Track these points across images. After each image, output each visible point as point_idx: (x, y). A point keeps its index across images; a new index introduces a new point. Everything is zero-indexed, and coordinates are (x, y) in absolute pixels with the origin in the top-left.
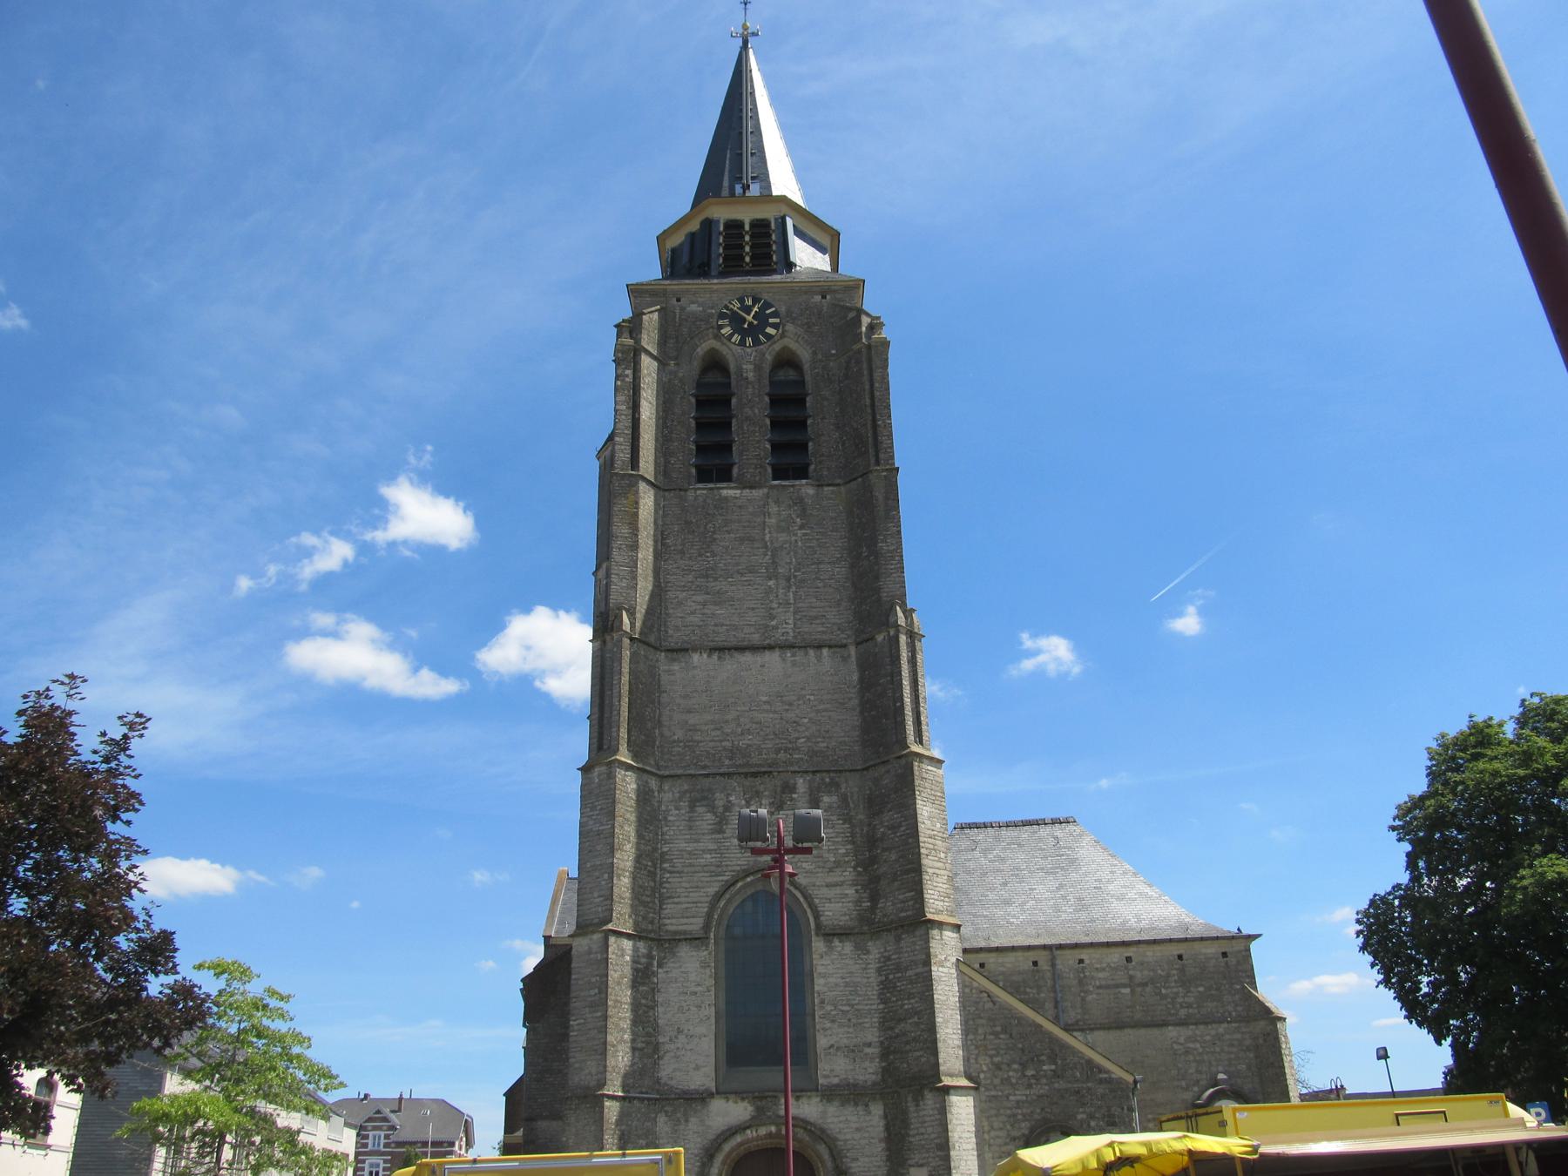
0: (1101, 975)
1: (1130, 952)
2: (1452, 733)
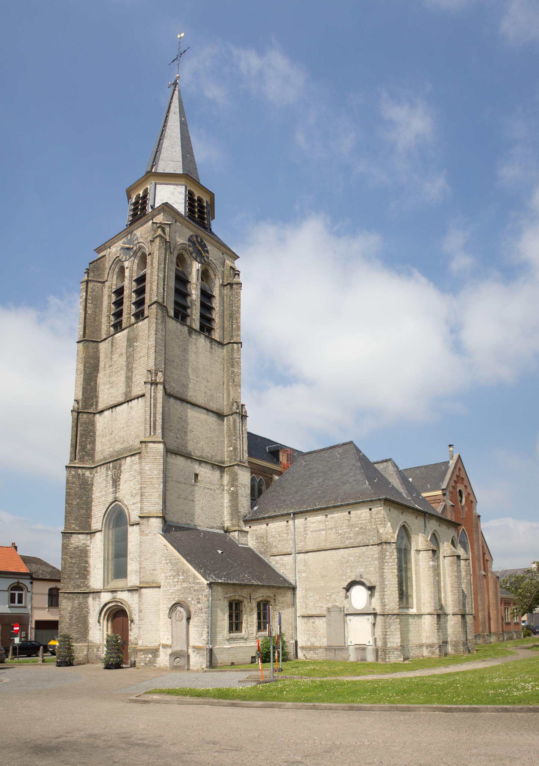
0: (314, 525)
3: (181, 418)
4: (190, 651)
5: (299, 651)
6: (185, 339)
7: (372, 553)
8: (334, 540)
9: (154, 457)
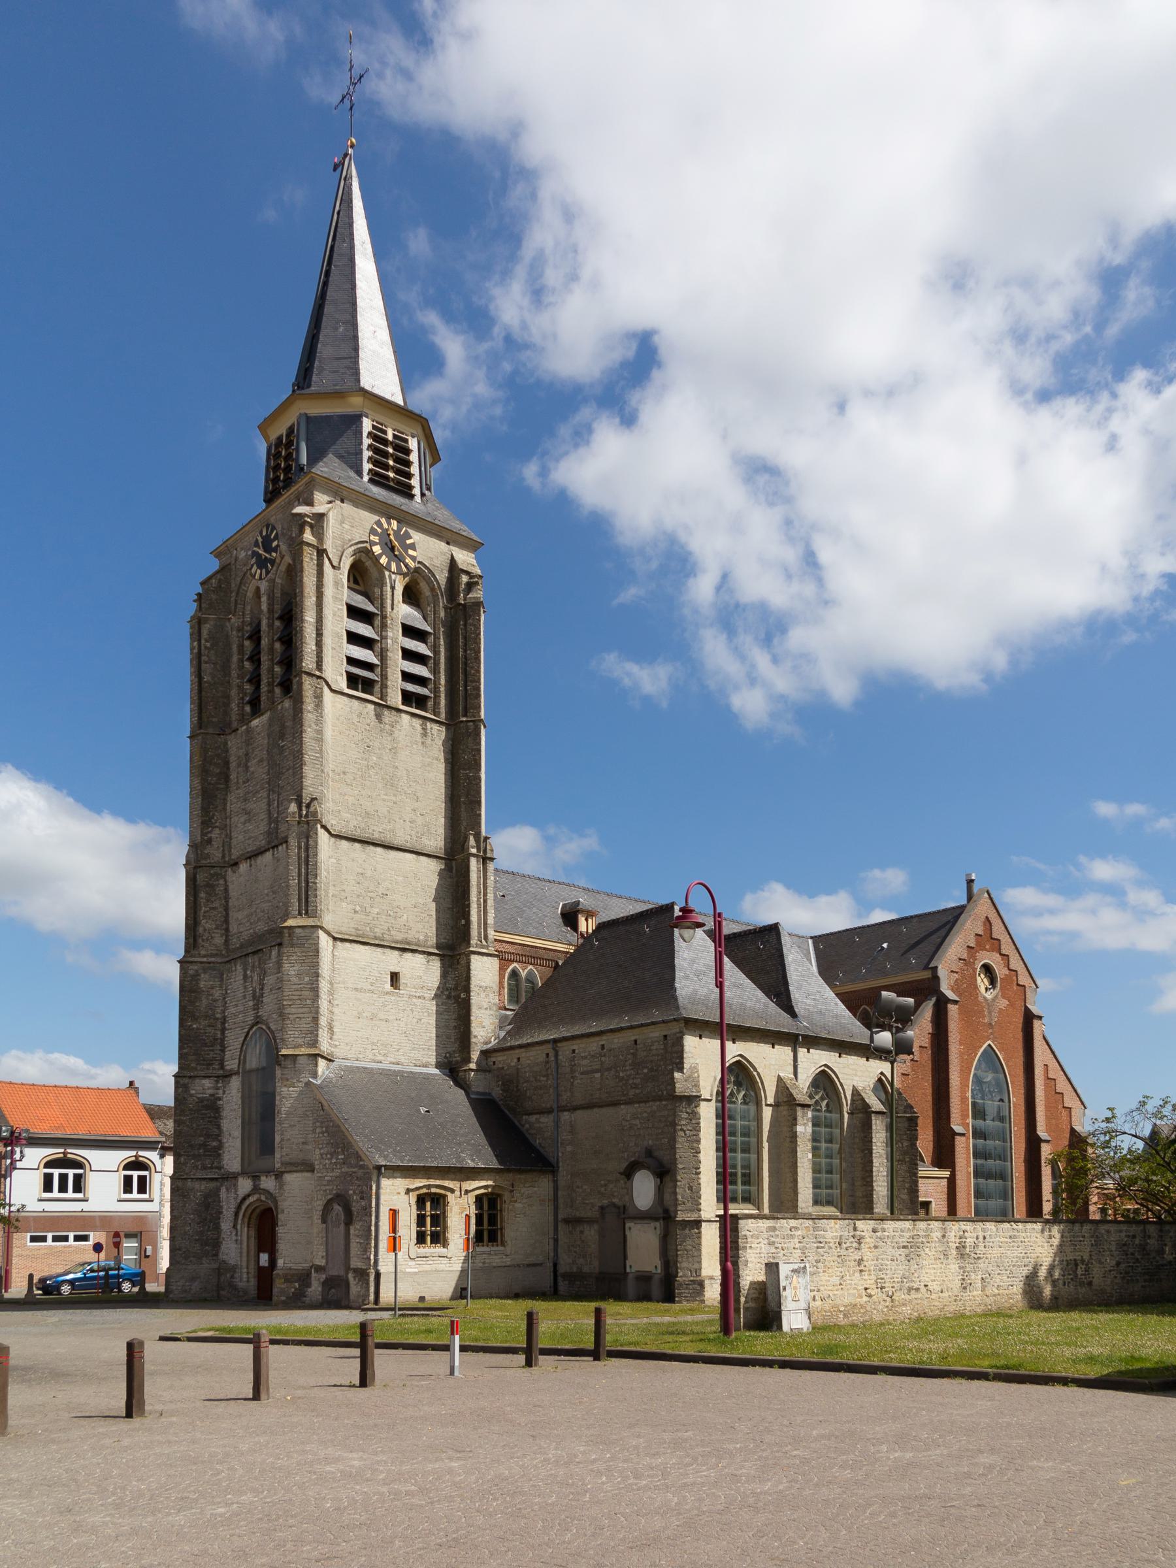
0: (585, 1062)
1: (603, 1040)
2: (305, 768)
3: (362, 874)
4: (351, 1276)
5: (560, 1279)
6: (368, 728)
7: (666, 1113)
8: (613, 1089)
9: (304, 954)
